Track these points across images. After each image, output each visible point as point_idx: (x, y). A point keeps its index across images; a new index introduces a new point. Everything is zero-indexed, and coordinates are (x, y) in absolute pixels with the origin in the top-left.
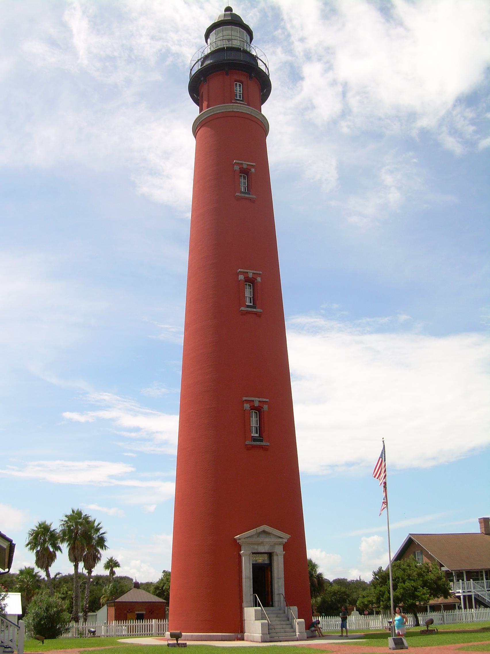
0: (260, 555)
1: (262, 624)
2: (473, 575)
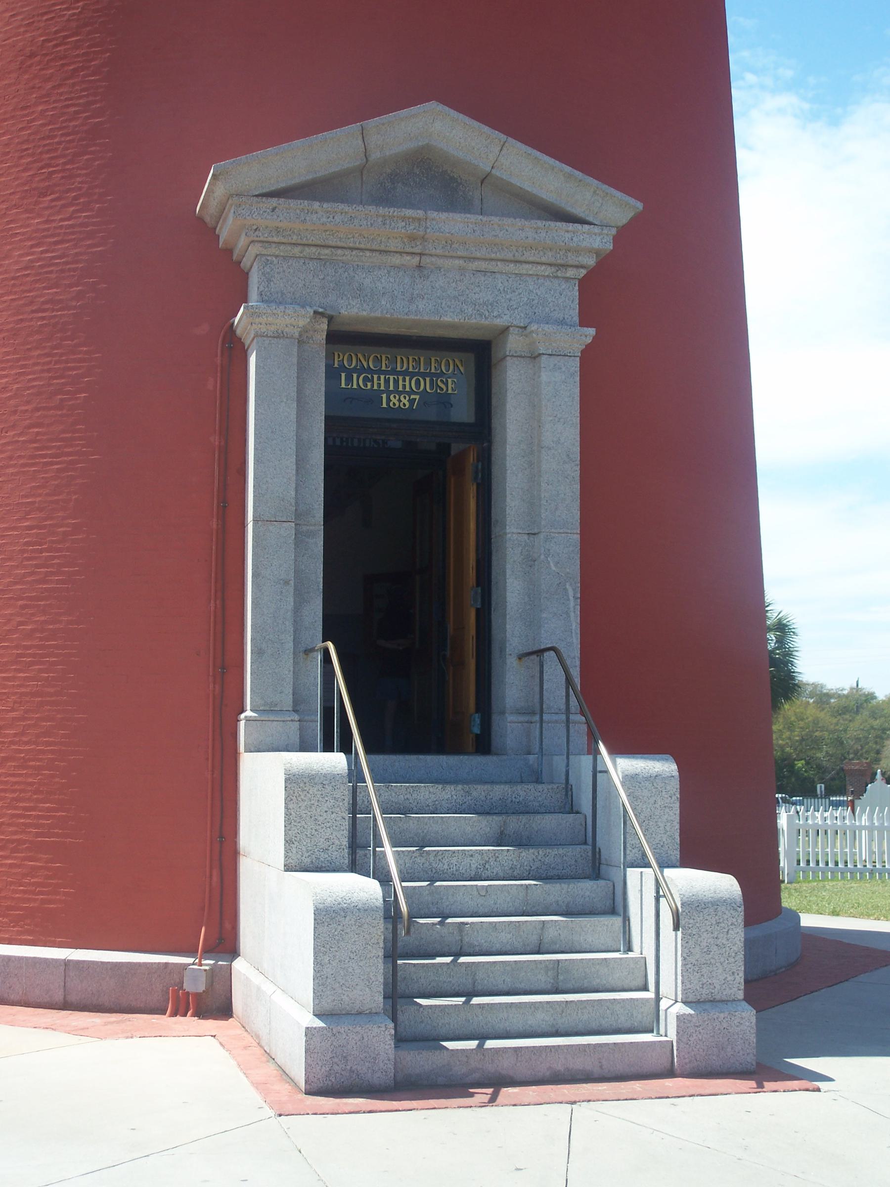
0: (406, 361)
1: (329, 919)
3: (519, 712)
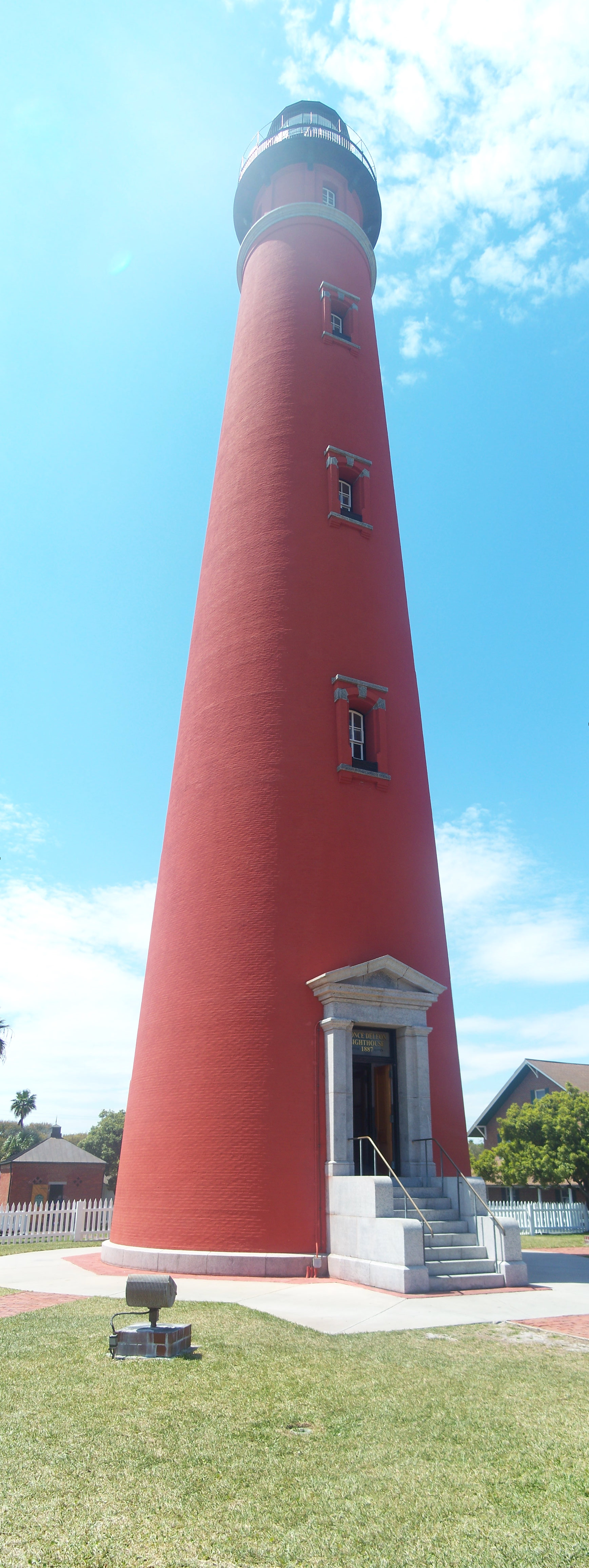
1: (408, 1231)
3: (413, 1161)
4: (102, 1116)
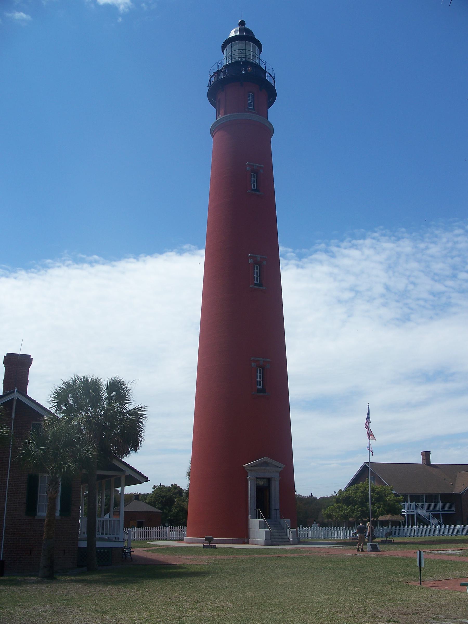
2: (416, 498)
4: (153, 488)
